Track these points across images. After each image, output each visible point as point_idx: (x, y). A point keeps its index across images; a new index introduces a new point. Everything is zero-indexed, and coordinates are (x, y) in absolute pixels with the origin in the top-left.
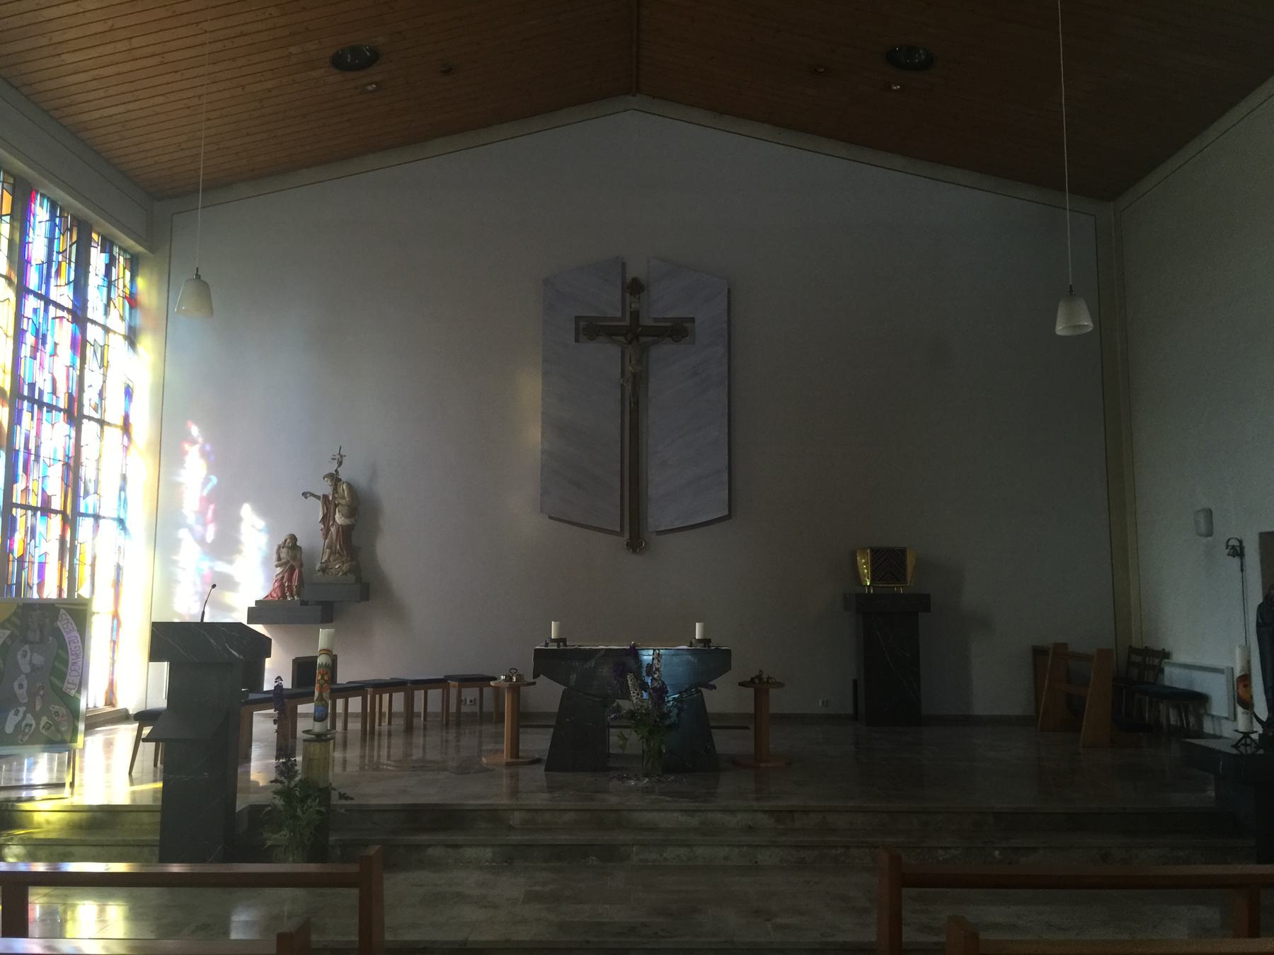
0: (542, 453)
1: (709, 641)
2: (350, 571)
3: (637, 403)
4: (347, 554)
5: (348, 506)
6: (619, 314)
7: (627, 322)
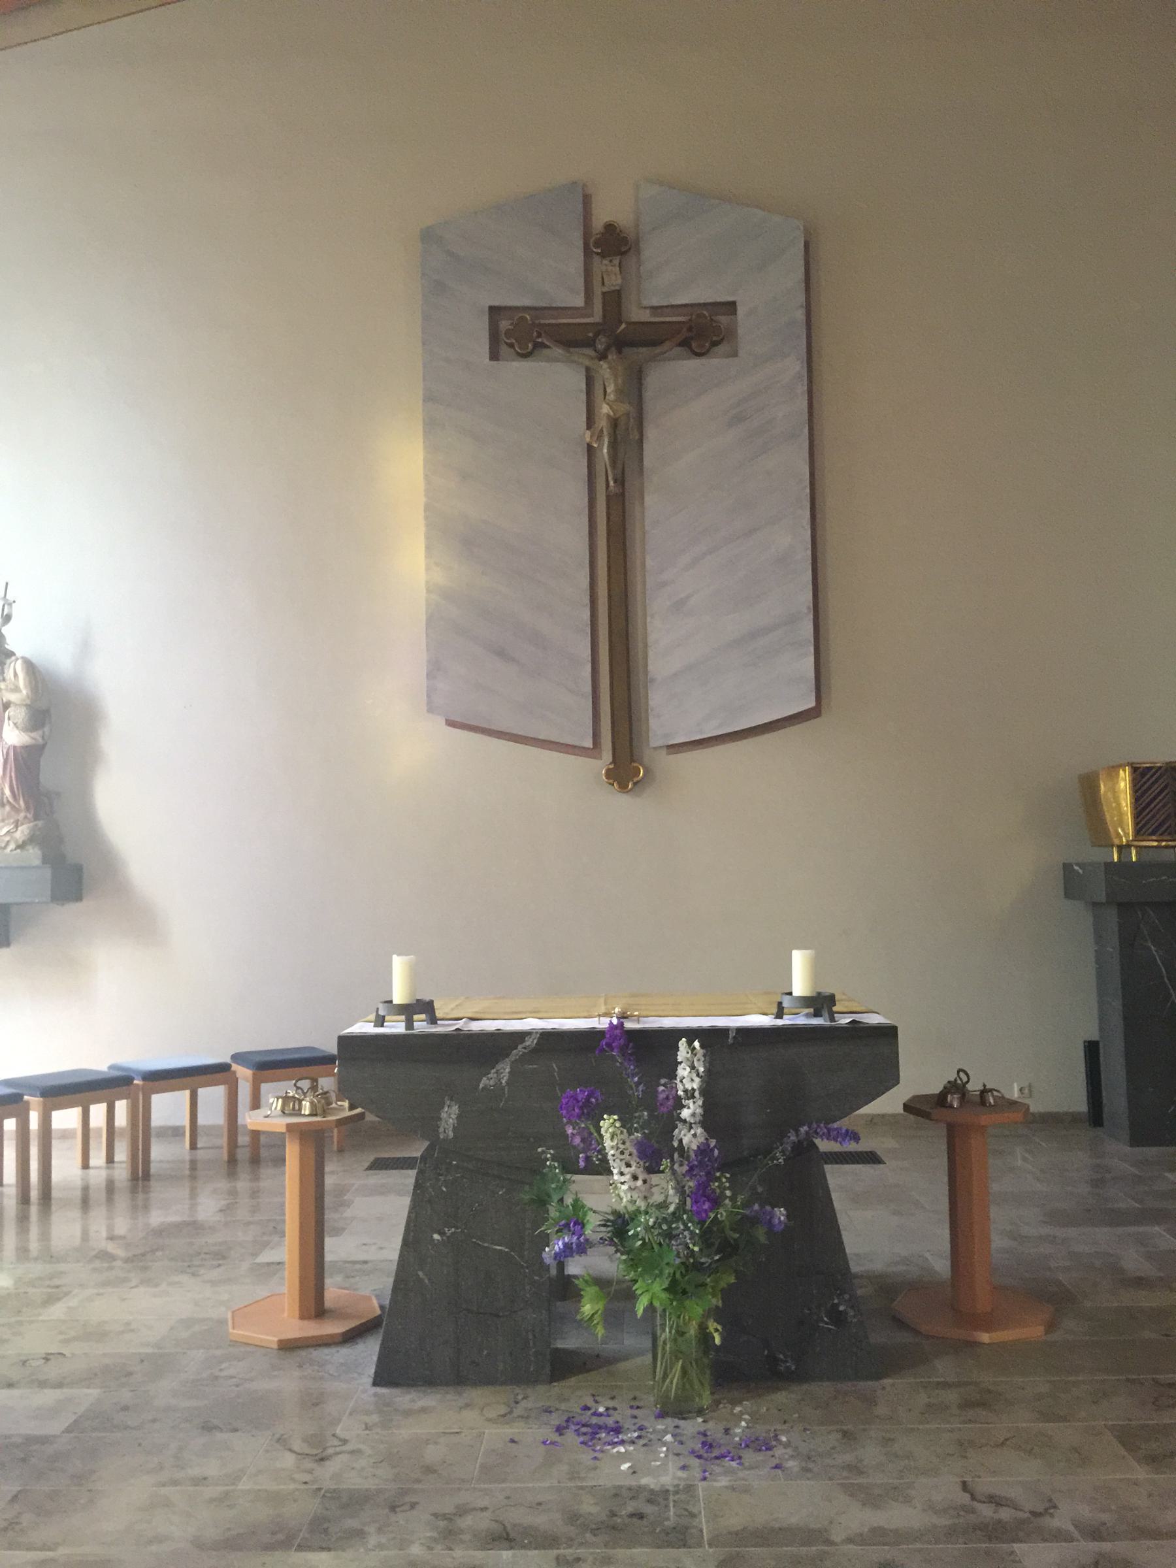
0: (428, 591)
1: (831, 1000)
2: (31, 840)
3: (621, 481)
4: (26, 803)
5: (26, 705)
6: (579, 301)
7: (597, 317)
